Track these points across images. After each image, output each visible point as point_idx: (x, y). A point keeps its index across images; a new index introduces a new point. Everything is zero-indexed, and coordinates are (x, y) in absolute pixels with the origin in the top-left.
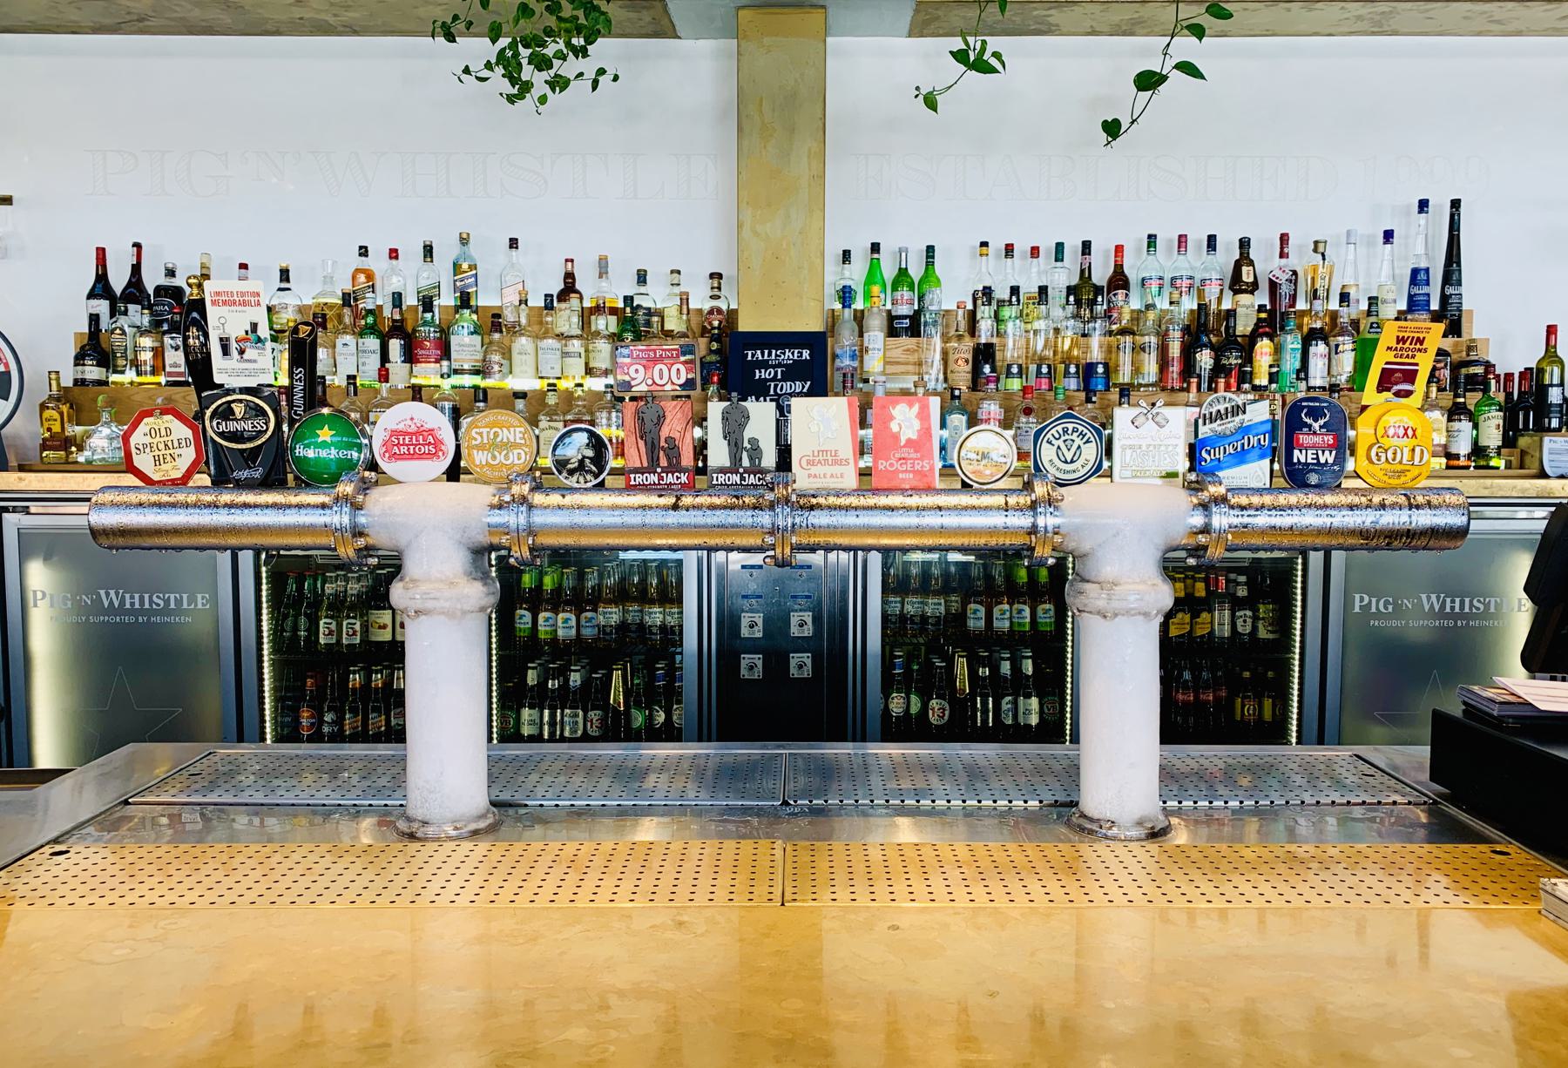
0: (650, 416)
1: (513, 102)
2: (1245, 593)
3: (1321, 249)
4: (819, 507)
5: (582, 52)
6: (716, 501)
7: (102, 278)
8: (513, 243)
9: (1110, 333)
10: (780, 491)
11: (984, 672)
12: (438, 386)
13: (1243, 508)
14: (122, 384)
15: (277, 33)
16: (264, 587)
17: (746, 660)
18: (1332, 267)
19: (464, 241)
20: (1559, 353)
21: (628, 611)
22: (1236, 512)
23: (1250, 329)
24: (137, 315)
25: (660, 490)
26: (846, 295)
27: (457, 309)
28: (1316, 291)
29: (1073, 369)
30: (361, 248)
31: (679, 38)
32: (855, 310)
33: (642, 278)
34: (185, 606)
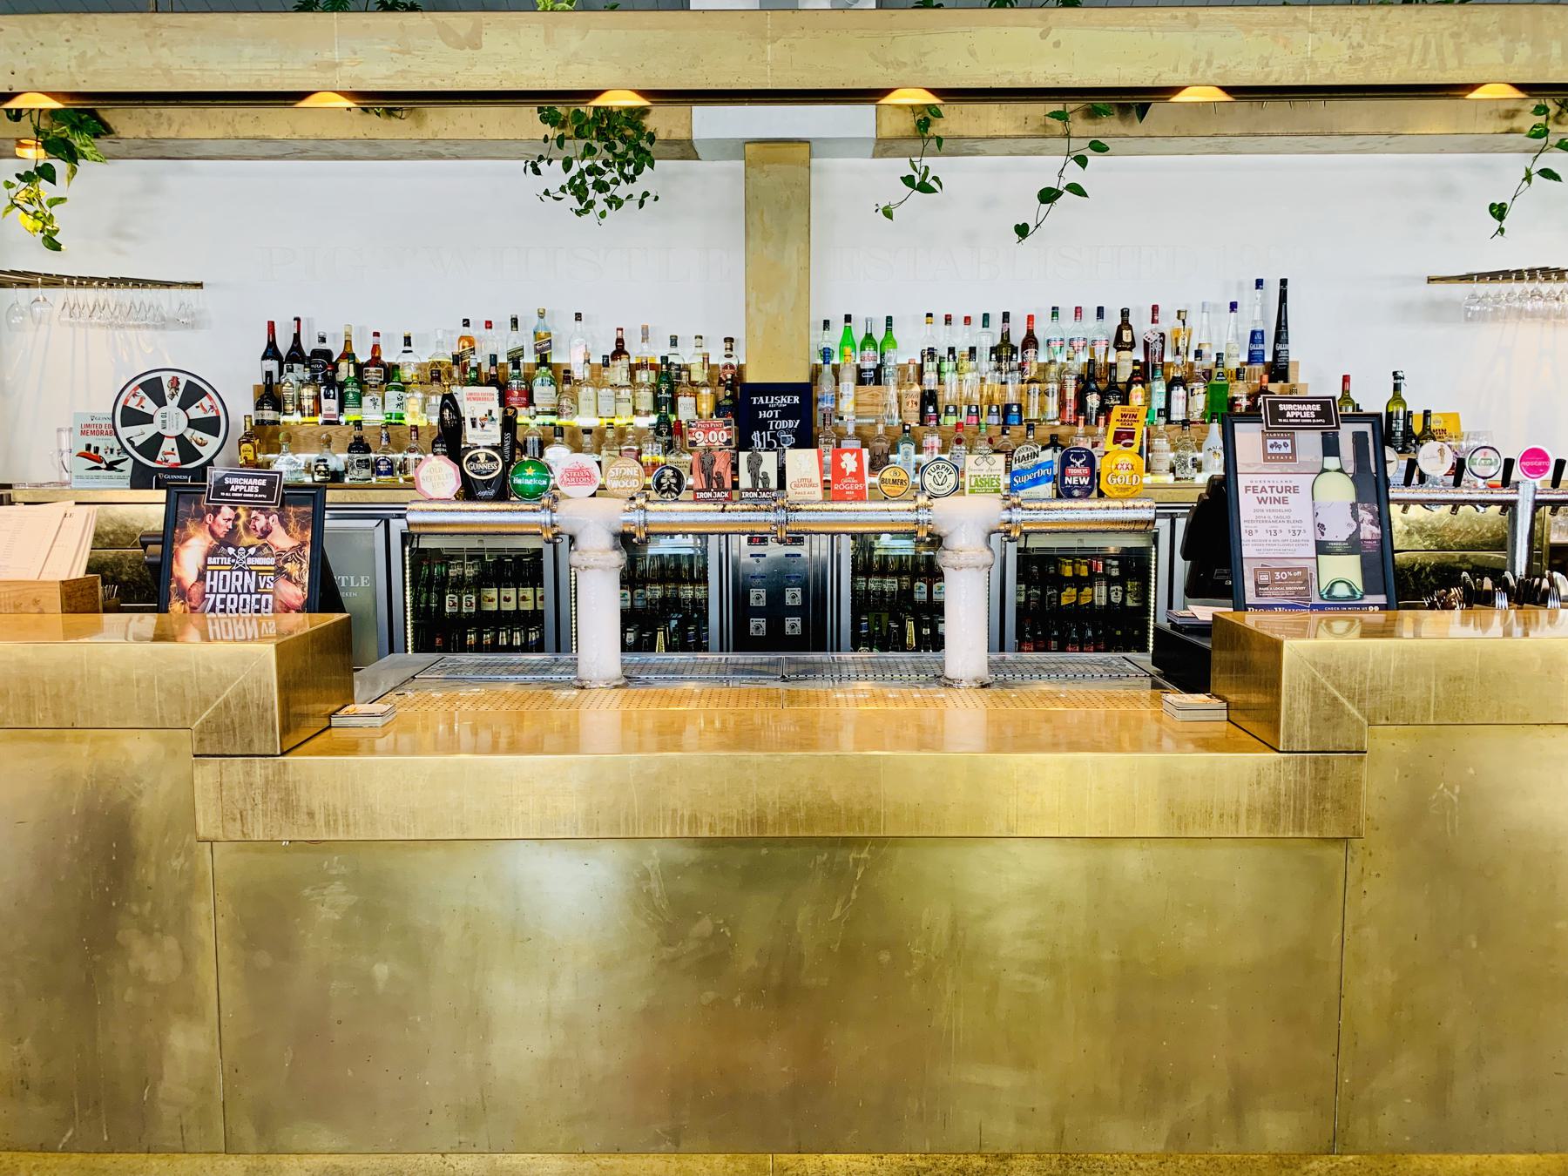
0: (707, 460)
1: (580, 215)
2: (1117, 574)
3: (1182, 317)
4: (800, 510)
5: (630, 179)
6: (745, 507)
7: (272, 344)
8: (578, 317)
9: (1023, 382)
10: (780, 502)
11: (926, 631)
12: (527, 425)
13: (1031, 510)
14: (290, 423)
15: (400, 158)
16: (408, 571)
17: (754, 622)
18: (1190, 330)
19: (541, 315)
20: (1351, 396)
21: (668, 589)
22: (1027, 512)
23: (1128, 377)
24: (300, 372)
25: (716, 501)
26: (826, 354)
27: (538, 366)
28: (1178, 348)
29: (994, 409)
30: (464, 320)
31: (699, 159)
32: (833, 365)
33: (674, 342)
34: (352, 585)
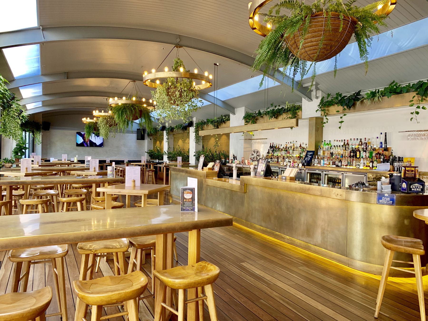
7: (271, 146)
